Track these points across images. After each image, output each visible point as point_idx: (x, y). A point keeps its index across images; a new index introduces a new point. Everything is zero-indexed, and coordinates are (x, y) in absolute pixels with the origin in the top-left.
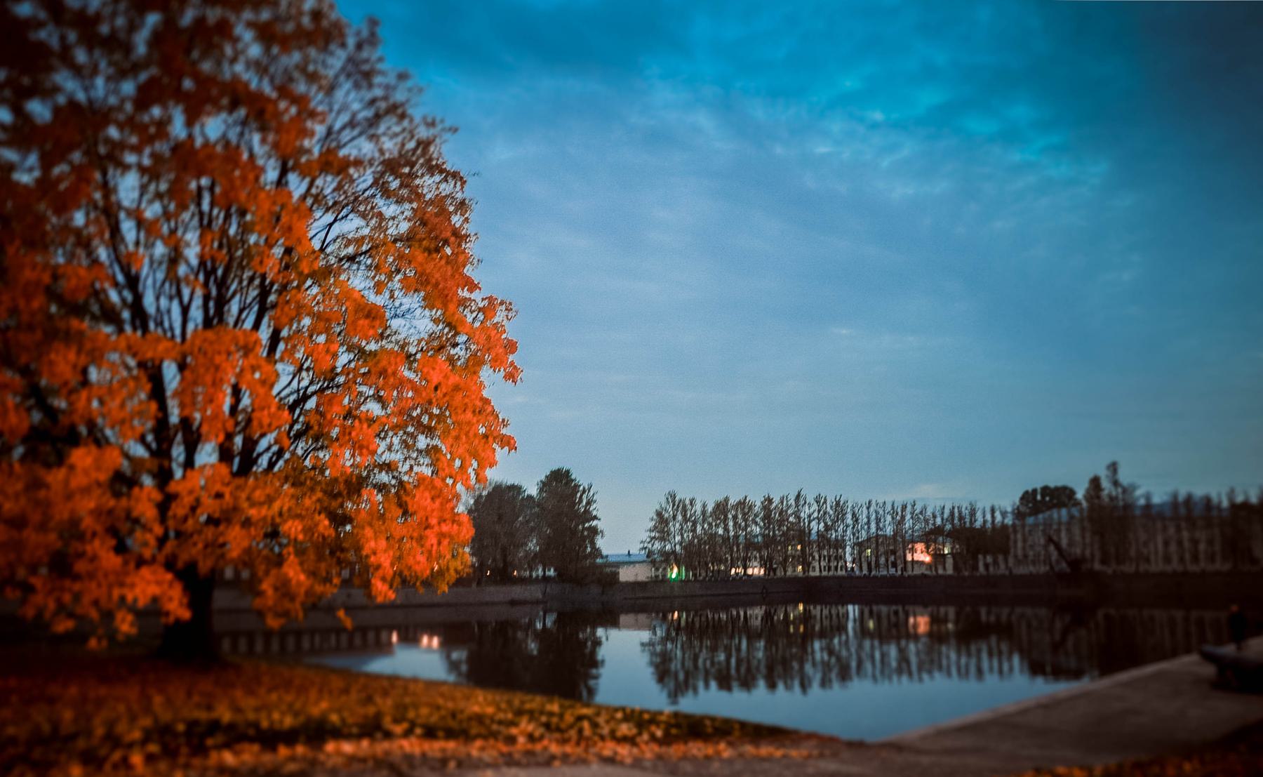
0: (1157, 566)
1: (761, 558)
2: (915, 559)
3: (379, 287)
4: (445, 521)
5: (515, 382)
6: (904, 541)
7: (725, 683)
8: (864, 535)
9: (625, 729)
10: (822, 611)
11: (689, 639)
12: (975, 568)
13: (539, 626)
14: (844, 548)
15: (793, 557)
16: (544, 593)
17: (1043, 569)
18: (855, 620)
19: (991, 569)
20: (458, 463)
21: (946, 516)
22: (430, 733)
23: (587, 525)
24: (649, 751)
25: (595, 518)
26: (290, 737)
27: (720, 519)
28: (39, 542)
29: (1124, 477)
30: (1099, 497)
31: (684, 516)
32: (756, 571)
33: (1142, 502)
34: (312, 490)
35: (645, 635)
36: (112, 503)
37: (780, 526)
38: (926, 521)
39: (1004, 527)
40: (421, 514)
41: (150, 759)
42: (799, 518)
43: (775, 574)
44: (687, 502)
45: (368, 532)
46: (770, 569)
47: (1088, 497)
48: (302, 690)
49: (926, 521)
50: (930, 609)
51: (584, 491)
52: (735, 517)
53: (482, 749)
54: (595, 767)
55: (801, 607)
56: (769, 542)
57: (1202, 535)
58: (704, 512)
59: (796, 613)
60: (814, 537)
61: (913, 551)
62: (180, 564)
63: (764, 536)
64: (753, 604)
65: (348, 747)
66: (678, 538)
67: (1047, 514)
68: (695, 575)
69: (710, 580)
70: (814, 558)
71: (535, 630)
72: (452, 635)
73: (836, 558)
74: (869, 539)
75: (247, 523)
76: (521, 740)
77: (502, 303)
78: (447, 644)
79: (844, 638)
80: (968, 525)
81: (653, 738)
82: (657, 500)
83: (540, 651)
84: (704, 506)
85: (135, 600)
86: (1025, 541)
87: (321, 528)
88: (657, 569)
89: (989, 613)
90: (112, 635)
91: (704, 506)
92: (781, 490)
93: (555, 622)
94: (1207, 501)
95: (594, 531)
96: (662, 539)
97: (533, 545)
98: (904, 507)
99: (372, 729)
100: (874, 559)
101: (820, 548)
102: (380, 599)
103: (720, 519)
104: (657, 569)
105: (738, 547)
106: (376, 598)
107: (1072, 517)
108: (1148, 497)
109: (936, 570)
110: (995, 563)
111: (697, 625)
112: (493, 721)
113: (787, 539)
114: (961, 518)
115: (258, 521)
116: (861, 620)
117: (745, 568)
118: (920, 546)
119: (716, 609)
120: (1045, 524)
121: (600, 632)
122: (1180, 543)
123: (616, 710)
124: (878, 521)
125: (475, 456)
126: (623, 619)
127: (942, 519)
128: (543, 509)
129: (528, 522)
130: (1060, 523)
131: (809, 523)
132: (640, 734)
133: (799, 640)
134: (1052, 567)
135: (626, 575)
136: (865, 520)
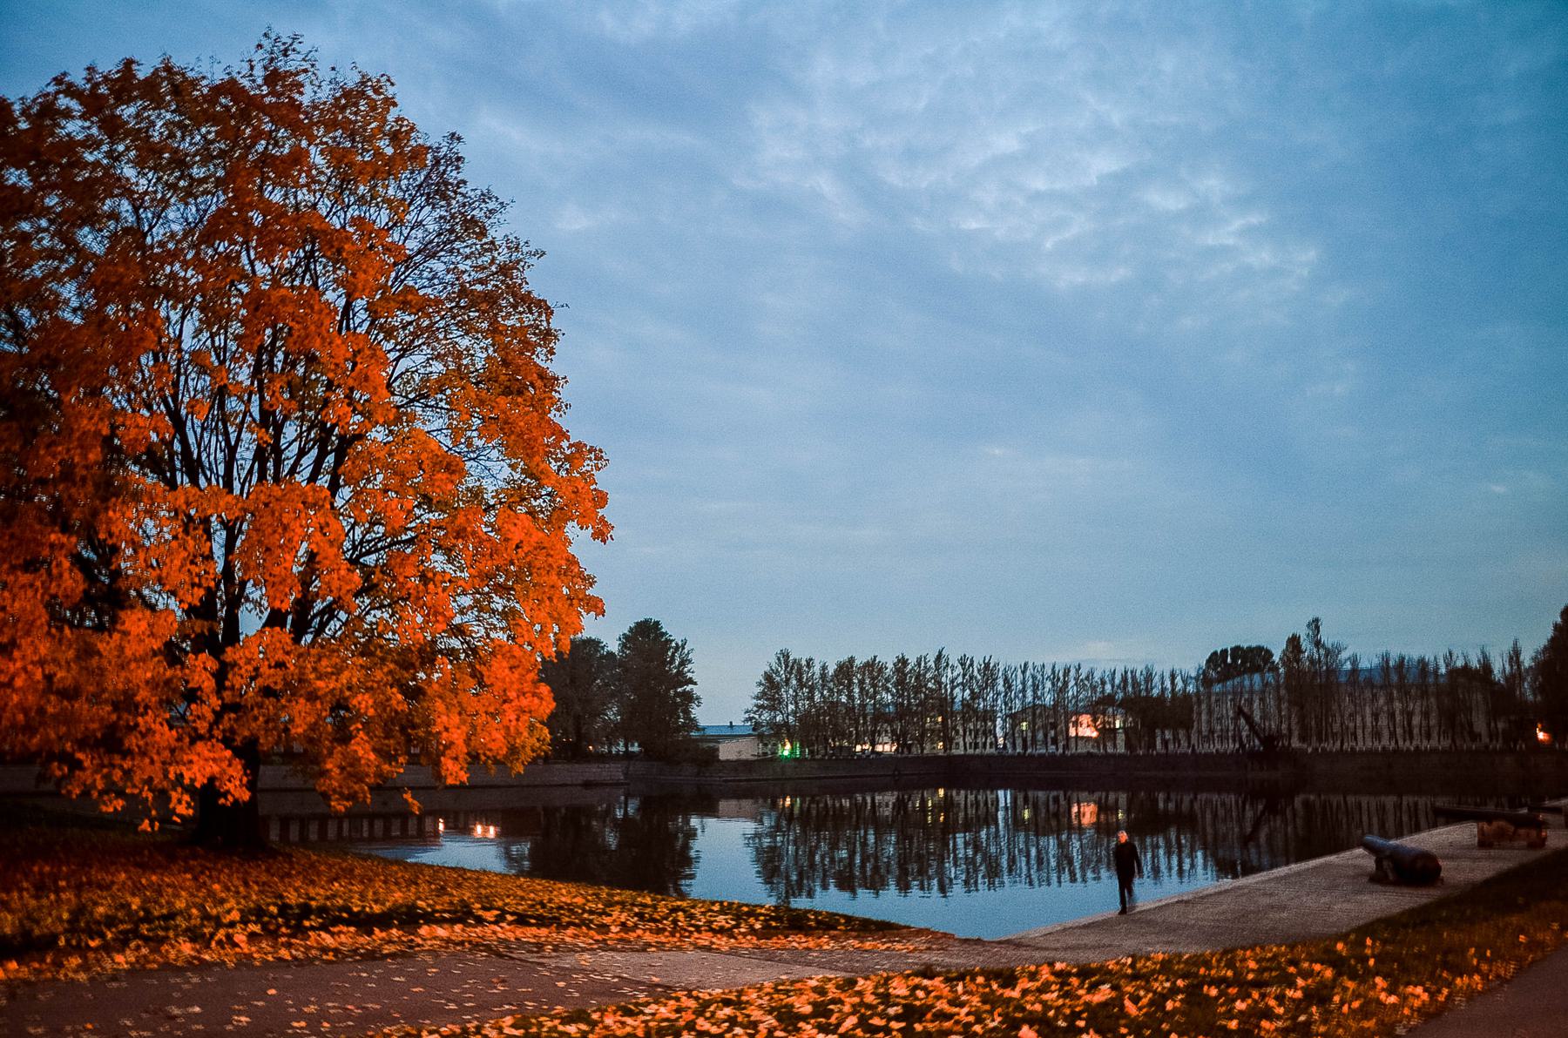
0: (1364, 744)
1: (894, 732)
2: (1080, 734)
3: (456, 433)
4: (524, 694)
5: (604, 541)
6: (1066, 713)
7: (847, 883)
8: (1018, 705)
9: (721, 921)
10: (966, 798)
11: (804, 831)
12: (1152, 745)
13: (619, 814)
14: (994, 722)
15: (933, 731)
16: (626, 774)
17: (1231, 746)
18: (1006, 808)
19: (1171, 747)
20: (538, 627)
21: (1117, 681)
22: (522, 920)
23: (679, 690)
24: (749, 942)
25: (691, 681)
26: (384, 921)
27: (842, 684)
28: (93, 715)
29: (1327, 637)
30: (1298, 661)
31: (799, 680)
32: (886, 747)
33: (1348, 666)
34: (383, 660)
35: (750, 827)
36: (169, 673)
37: (916, 693)
38: (1094, 688)
39: (1186, 696)
40: (498, 686)
41: (252, 937)
42: (940, 683)
43: (910, 752)
44: (804, 663)
45: (439, 705)
46: (903, 746)
47: (1286, 660)
48: (367, 881)
49: (1094, 688)
50: (1096, 795)
51: (677, 647)
52: (861, 682)
53: (575, 936)
54: (692, 954)
55: (941, 792)
56: (903, 712)
57: (1416, 707)
58: (823, 676)
59: (936, 799)
60: (957, 706)
61: (1076, 724)
62: (238, 740)
63: (895, 704)
64: (883, 789)
65: (441, 932)
66: (791, 707)
67: (1237, 680)
68: (811, 752)
69: (830, 759)
70: (957, 732)
71: (615, 819)
72: (512, 825)
73: (985, 733)
74: (1024, 710)
75: (312, 697)
76: (614, 929)
77: (590, 451)
78: (509, 833)
79: (993, 829)
80: (1143, 694)
81: (752, 931)
82: (766, 661)
83: (619, 846)
84: (824, 668)
85: (193, 780)
86: (1210, 713)
87: (394, 702)
88: (766, 745)
89: (1167, 800)
90: (166, 817)
91: (824, 668)
92: (918, 649)
93: (638, 810)
94: (1422, 663)
95: (689, 698)
96: (772, 708)
97: (612, 714)
98: (1067, 672)
99: (462, 915)
100: (1030, 734)
101: (965, 721)
102: (450, 781)
103: (842, 684)
104: (766, 745)
105: (865, 719)
106: (446, 777)
107: (1266, 685)
108: (1354, 660)
109: (1105, 748)
110: (1176, 739)
111: (814, 812)
112: (584, 911)
113: (925, 709)
114: (1135, 684)
115: (326, 695)
116: (1015, 808)
117: (873, 744)
118: (1085, 719)
119: (837, 793)
120: (1234, 693)
121: (694, 822)
122: (1392, 716)
123: (713, 903)
124: (1035, 688)
125: (558, 621)
126: (723, 805)
127: (1113, 686)
128: (627, 670)
129: (607, 685)
130: (1251, 692)
131: (952, 689)
132: (737, 926)
133: (939, 833)
134: (1242, 745)
135: (727, 752)
136: (1020, 687)
